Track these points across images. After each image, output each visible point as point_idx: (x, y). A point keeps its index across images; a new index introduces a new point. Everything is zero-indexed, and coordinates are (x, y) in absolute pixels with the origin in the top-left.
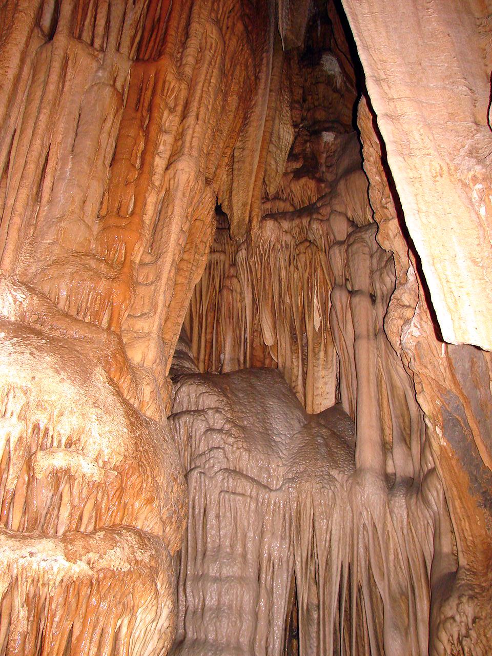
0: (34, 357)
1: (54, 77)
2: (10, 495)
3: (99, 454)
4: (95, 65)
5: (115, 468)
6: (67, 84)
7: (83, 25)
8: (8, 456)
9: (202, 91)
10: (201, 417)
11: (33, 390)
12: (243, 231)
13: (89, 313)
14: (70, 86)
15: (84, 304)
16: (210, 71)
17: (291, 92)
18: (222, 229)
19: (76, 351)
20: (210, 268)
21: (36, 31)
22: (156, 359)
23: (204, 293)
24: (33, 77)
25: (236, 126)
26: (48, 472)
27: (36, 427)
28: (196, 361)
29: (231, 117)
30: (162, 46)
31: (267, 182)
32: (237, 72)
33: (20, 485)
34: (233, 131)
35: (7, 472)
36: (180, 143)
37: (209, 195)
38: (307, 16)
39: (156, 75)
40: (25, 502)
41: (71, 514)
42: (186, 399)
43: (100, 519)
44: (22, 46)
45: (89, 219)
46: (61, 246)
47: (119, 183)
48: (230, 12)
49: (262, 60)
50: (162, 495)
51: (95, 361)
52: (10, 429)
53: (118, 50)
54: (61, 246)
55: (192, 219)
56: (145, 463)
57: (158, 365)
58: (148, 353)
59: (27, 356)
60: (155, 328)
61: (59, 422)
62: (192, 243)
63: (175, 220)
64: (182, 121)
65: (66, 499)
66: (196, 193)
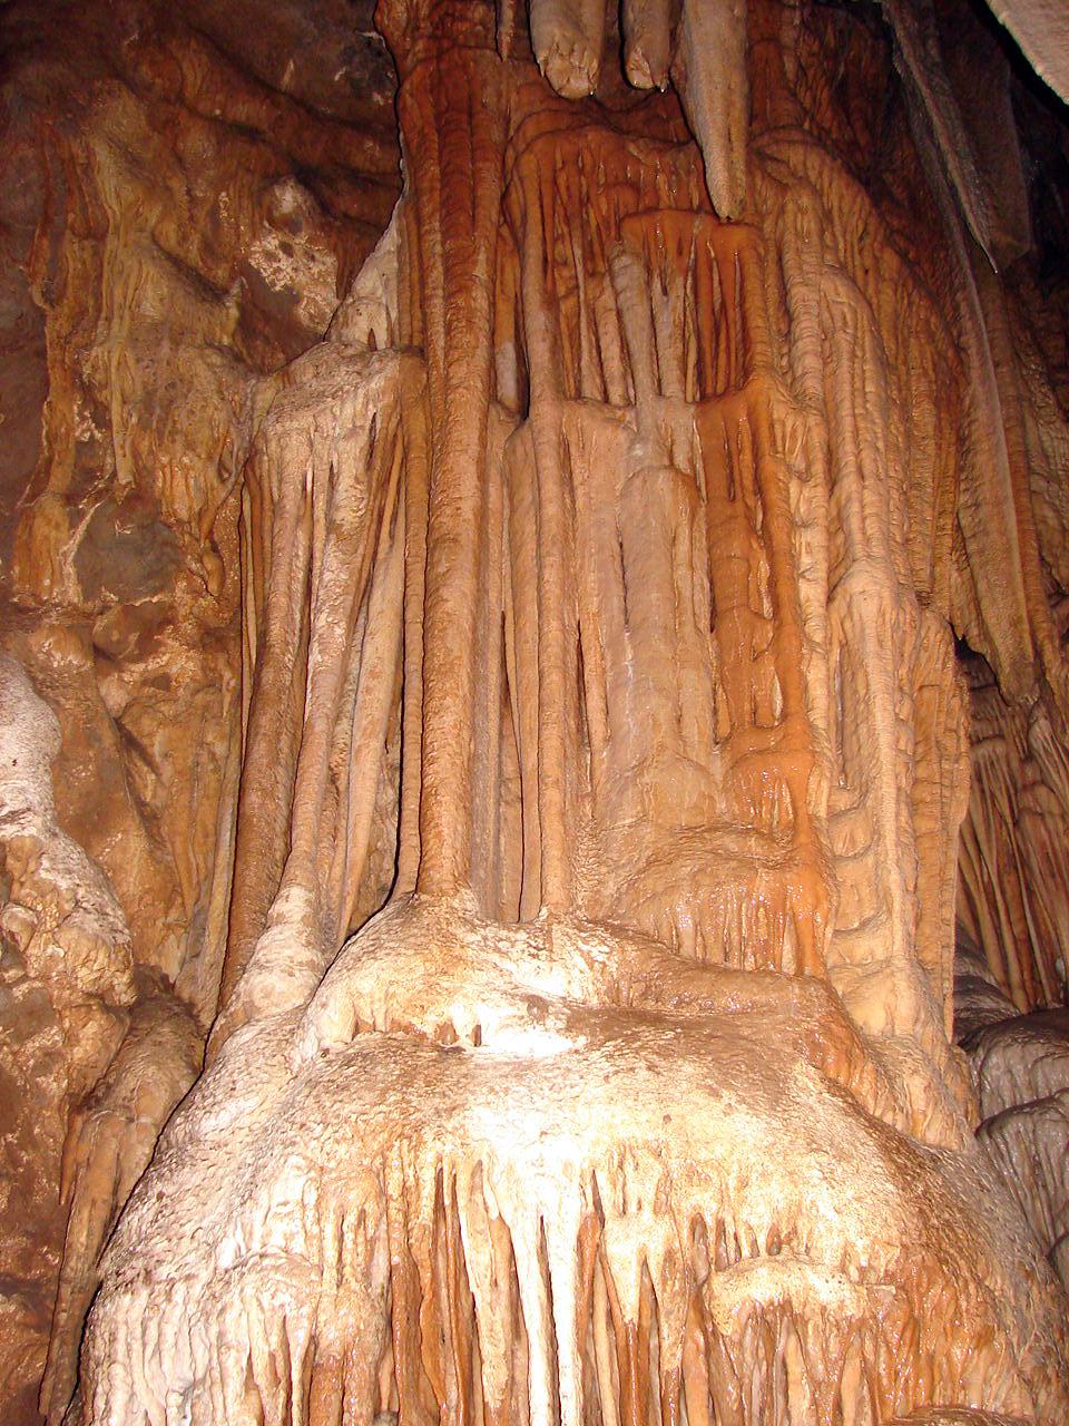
0: (658, 1073)
1: (551, 488)
2: (673, 1386)
3: (846, 1254)
4: (622, 437)
5: (890, 1277)
6: (580, 492)
7: (580, 369)
8: (651, 1298)
9: (854, 416)
10: (1052, 1115)
11: (672, 1145)
12: (1029, 680)
13: (749, 951)
14: (587, 494)
15: (734, 934)
16: (858, 371)
17: (1041, 351)
18: (980, 689)
19: (744, 1038)
20: (980, 780)
21: (493, 412)
22: (918, 1013)
23: (982, 837)
24: (511, 500)
25: (946, 465)
26: (744, 1316)
27: (697, 1223)
28: (1004, 990)
29: (931, 449)
30: (745, 355)
31: (1049, 559)
32: (914, 352)
33: (691, 1355)
34: (944, 475)
35: (655, 1332)
36: (840, 539)
37: (933, 629)
38: (1024, 184)
39: (749, 415)
40: (710, 1392)
41: (814, 1402)
42: (1005, 1082)
43: (883, 1402)
44: (474, 448)
45: (698, 753)
46: (657, 825)
47: (738, 660)
48: (861, 239)
49: (956, 308)
50: (1009, 1319)
51: (789, 1050)
52: (642, 1239)
53: (660, 393)
54: (657, 825)
55: (912, 689)
56: (952, 1251)
57: (925, 1024)
58: (897, 1003)
59: (643, 1074)
60: (899, 944)
61: (743, 1201)
62: (927, 739)
63: (879, 702)
64: (831, 491)
65: (796, 1369)
66: (904, 632)
